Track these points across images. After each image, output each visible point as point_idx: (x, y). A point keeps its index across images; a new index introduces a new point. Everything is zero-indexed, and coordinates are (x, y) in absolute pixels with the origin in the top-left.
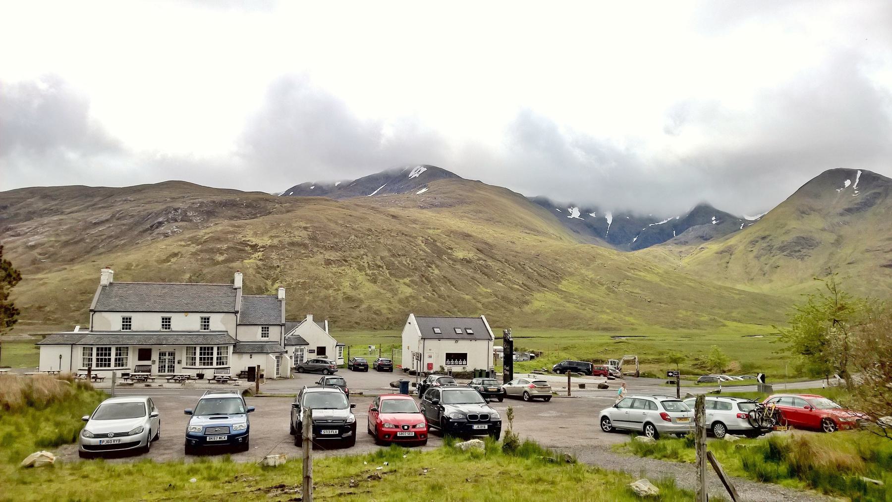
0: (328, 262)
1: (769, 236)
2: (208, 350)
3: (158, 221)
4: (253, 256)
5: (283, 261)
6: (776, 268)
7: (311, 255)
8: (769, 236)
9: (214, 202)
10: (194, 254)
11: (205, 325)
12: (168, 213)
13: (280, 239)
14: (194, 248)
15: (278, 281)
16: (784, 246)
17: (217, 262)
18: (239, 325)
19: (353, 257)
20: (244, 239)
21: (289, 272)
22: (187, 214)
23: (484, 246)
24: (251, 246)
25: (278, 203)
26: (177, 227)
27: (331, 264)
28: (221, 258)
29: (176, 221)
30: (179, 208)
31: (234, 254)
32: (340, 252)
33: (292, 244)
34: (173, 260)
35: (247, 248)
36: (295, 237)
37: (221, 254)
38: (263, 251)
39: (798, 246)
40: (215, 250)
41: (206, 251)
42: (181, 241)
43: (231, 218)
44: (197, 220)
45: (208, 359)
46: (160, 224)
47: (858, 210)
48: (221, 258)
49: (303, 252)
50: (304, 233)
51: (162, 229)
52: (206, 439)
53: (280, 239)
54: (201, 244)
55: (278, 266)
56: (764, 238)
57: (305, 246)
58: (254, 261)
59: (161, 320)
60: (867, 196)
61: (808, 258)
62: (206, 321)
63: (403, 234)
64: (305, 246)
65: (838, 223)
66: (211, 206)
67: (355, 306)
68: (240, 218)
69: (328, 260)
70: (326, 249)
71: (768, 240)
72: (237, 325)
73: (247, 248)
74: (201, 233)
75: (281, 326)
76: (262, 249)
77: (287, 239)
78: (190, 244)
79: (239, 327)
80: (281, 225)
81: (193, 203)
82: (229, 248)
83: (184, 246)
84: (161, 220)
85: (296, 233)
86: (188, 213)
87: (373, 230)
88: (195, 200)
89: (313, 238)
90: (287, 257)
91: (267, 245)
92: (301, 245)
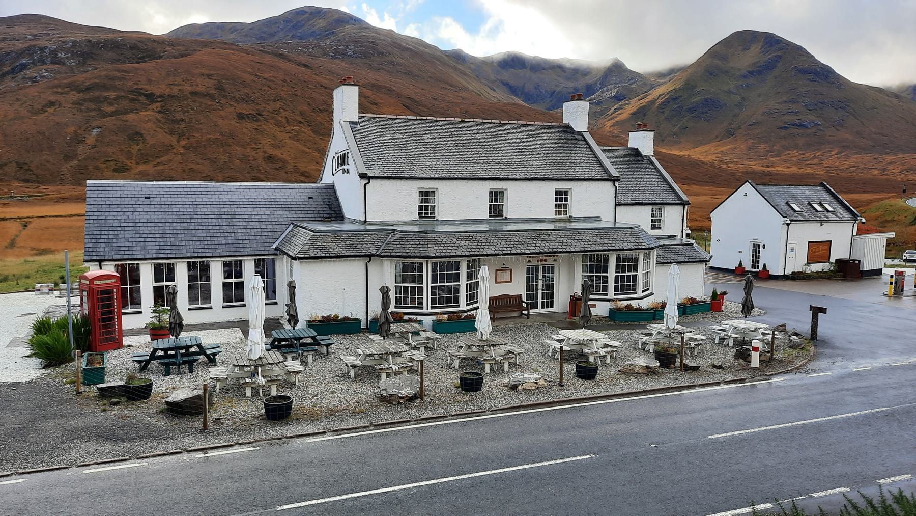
0: (241, 116)
1: (681, 97)
2: (450, 269)
3: (21, 62)
4: (149, 107)
5: (187, 114)
6: (685, 129)
7: (220, 108)
8: (681, 97)
9: (89, 41)
10: (78, 103)
11: (496, 200)
12: (33, 53)
13: (180, 87)
14: (74, 96)
15: (184, 137)
16: (693, 108)
17: (107, 113)
18: (620, 205)
19: (269, 111)
20: (136, 86)
21: (197, 126)
22: (57, 55)
23: (409, 102)
24: (145, 95)
25: (168, 45)
26: (47, 71)
27: (244, 118)
28: (109, 109)
29: (44, 63)
30: (46, 48)
31: (125, 104)
32: (253, 105)
33: (194, 93)
34: (51, 110)
35: (140, 98)
36: (198, 85)
37: (111, 104)
38: (161, 102)
39: (706, 108)
40: (102, 100)
41: (90, 100)
42: (56, 87)
43: (113, 61)
44: (72, 62)
45: (449, 292)
46: (23, 67)
47: (760, 73)
48: (109, 109)
49: (210, 103)
50: (210, 83)
51: (28, 73)
52: (182, 353)
53: (180, 87)
54: (83, 91)
55: (183, 120)
56: (675, 99)
57: (212, 97)
58: (152, 113)
59: (417, 197)
60: (769, 59)
61: (713, 120)
62: (562, 197)
63: (322, 86)
64: (212, 97)
65: (742, 85)
66: (87, 46)
67: (280, 167)
68: (124, 62)
69: (241, 113)
70: (236, 100)
71: (678, 101)
72: (617, 205)
73: (140, 98)
74: (81, 78)
75: (684, 205)
76: (159, 99)
77: (188, 88)
78: (69, 91)
79: (618, 208)
80: (179, 71)
81: (63, 42)
82: (118, 98)
83: (62, 93)
84: (24, 61)
85: (199, 81)
86: (59, 55)
87: (288, 81)
88: (65, 39)
89: (220, 88)
90: (192, 109)
91: (165, 94)
92: (206, 96)
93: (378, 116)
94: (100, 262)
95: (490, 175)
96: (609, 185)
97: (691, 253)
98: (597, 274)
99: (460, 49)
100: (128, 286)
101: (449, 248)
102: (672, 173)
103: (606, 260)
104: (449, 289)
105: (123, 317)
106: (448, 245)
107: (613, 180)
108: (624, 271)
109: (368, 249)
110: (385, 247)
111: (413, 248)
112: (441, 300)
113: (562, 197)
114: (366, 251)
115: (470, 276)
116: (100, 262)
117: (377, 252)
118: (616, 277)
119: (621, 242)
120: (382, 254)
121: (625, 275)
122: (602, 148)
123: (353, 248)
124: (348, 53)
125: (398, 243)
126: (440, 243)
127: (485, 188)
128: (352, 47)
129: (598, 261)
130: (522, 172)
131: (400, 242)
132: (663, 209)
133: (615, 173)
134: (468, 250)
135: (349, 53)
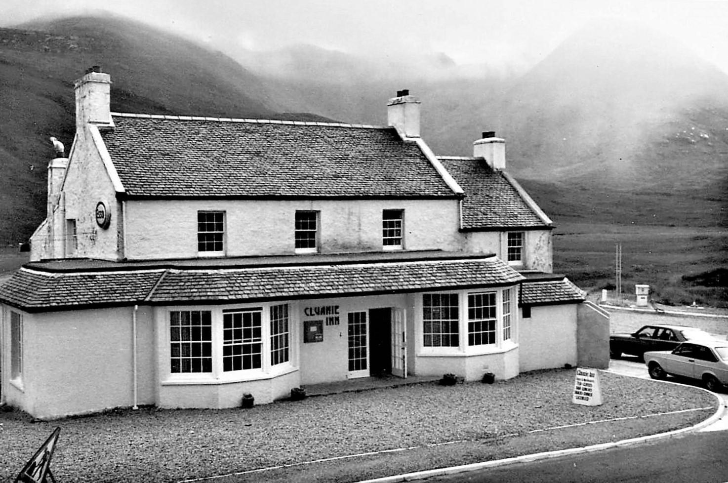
62: (392, 220)
93: (124, 115)
94: (247, 402)
95: (296, 192)
96: (451, 205)
97: (563, 290)
98: (434, 320)
99: (219, 53)
100: (201, 326)
101: (246, 288)
102: (530, 189)
103: (455, 300)
104: (247, 349)
105: (131, 255)
106: (245, 284)
107: (458, 197)
108: (479, 317)
109: (133, 294)
110: (156, 290)
111: (196, 290)
112: (187, 364)
113: (392, 220)
114: (130, 297)
115: (274, 328)
116: (247, 402)
117: (145, 298)
118: (470, 325)
119: (474, 276)
120: (154, 300)
121: (487, 322)
122: (439, 157)
123: (112, 294)
124: (69, 45)
125: (176, 284)
126: (234, 281)
127: (289, 210)
128: (76, 38)
129: (238, 324)
130: (339, 187)
131: (178, 283)
132: (522, 235)
133: (457, 189)
134: (273, 290)
135: (72, 46)
